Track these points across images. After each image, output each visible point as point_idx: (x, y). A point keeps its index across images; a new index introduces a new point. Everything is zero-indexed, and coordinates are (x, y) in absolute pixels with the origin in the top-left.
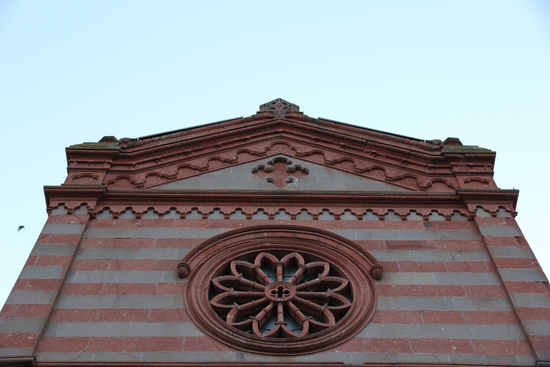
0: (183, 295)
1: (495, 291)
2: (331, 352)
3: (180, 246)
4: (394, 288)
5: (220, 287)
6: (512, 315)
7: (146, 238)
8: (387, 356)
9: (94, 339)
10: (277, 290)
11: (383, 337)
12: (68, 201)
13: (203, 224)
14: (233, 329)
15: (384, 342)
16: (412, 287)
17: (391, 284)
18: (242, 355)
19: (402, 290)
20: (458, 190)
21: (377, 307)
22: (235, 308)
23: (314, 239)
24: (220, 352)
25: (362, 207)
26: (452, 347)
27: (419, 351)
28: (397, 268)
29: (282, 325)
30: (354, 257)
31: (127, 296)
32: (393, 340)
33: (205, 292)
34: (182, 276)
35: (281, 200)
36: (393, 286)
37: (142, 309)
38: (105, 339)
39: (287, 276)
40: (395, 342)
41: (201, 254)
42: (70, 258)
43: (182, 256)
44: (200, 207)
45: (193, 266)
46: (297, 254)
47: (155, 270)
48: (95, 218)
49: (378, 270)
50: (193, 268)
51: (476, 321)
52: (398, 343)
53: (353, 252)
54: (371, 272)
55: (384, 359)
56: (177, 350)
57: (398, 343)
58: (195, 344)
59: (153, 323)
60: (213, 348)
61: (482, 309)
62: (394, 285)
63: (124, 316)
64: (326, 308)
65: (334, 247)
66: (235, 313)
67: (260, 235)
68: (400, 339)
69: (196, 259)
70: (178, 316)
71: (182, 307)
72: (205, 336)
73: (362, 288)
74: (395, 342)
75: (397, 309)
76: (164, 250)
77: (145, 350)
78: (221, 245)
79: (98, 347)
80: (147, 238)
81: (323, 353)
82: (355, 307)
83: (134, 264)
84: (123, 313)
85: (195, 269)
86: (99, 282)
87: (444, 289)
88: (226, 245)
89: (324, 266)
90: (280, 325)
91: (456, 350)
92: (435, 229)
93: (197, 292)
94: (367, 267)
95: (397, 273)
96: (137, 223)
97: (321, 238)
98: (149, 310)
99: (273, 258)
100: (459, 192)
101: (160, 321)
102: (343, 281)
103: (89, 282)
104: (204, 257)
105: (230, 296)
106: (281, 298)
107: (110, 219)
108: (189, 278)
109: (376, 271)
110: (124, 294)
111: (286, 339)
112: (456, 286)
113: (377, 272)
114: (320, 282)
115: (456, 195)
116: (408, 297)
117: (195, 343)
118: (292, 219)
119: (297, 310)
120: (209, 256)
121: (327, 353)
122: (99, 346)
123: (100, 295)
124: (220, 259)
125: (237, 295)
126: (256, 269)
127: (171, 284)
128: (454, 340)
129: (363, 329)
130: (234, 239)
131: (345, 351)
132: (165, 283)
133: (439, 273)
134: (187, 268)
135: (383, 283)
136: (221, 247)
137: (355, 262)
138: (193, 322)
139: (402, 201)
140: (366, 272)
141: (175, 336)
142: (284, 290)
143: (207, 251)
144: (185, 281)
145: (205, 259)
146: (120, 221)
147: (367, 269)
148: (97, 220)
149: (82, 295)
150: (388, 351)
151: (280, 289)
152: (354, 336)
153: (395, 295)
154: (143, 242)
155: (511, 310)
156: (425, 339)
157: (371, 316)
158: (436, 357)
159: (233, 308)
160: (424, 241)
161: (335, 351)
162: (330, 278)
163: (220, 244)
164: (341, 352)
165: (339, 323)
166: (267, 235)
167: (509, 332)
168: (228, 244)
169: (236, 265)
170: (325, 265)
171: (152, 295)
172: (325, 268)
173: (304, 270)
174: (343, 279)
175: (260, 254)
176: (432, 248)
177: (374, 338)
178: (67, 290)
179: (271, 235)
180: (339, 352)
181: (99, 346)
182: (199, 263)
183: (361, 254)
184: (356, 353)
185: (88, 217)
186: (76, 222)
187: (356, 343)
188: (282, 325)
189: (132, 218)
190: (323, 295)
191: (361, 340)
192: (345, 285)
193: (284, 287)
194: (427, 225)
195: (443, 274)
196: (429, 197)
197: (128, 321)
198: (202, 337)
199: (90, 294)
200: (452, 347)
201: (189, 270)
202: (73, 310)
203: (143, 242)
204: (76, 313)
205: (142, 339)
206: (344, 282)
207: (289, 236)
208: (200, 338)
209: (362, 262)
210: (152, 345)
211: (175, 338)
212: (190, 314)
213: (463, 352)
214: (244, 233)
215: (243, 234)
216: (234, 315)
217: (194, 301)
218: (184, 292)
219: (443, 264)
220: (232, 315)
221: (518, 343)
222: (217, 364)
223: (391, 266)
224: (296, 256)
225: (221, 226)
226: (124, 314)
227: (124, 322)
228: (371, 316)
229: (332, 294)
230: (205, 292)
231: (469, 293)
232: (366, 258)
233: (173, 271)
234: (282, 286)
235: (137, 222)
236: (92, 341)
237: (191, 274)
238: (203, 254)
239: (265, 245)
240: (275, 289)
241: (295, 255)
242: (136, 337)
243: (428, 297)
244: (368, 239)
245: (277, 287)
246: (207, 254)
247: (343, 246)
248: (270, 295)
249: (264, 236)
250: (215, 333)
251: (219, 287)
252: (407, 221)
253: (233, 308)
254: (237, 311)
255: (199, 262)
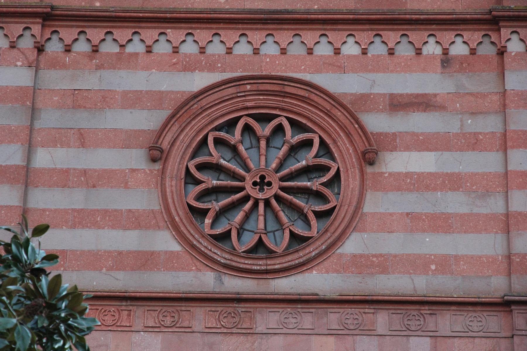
0: (157, 190)
1: (497, 182)
2: (308, 273)
3: (149, 104)
4: (386, 178)
5: (196, 176)
6: (505, 219)
7: (108, 90)
8: (364, 278)
9: (73, 252)
10: (258, 181)
11: (363, 252)
12: (7, 24)
13: (174, 64)
14: (212, 240)
15: (363, 260)
16: (406, 176)
17: (384, 170)
18: (221, 277)
19: (395, 182)
20: (491, 10)
21: (364, 209)
22: (213, 209)
23: (305, 96)
24: (199, 273)
25: (369, 31)
26: (431, 265)
27: (397, 272)
28: (395, 144)
29: (261, 234)
30: (348, 127)
31: (97, 190)
32: (374, 256)
33: (181, 182)
34: (154, 160)
35: (269, 21)
36: (386, 175)
37: (116, 210)
38: (83, 252)
39: (271, 147)
40: (375, 259)
41: (174, 125)
42: (28, 131)
43: (152, 123)
44: (169, 32)
45: (165, 145)
46: (284, 120)
47: (124, 148)
48: (43, 50)
49: (371, 155)
50: (165, 148)
51: (464, 228)
52: (377, 261)
53: (348, 121)
54: (364, 154)
55: (361, 283)
56: (156, 270)
57: (377, 261)
58: (173, 261)
59: (129, 231)
60: (191, 267)
61: (476, 210)
62: (387, 172)
63: (98, 221)
64: (310, 209)
65: (327, 110)
66: (213, 216)
67: (242, 88)
68: (381, 255)
69: (169, 133)
70: (154, 221)
71: (157, 208)
72: (183, 250)
73: (351, 179)
74: (375, 259)
75: (384, 211)
76: (131, 112)
77: (124, 269)
78: (196, 108)
79: (78, 265)
80: (110, 90)
81: (300, 274)
82: (341, 206)
83: (100, 137)
84: (97, 215)
85: (169, 147)
86: (65, 167)
87: (441, 179)
88: (202, 106)
89: (313, 139)
90: (259, 234)
91: (435, 269)
92: (452, 72)
93: (172, 186)
94: (361, 148)
95: (394, 153)
96: (94, 61)
97: (313, 95)
98: (123, 211)
99: (256, 127)
100: (493, 13)
101: (136, 228)
102: (332, 166)
103: (54, 167)
104: (177, 128)
105: (208, 188)
106: (263, 193)
107: (61, 52)
108: (163, 161)
109: (369, 157)
110: (94, 186)
111: (264, 256)
112: (456, 174)
113: (369, 158)
114: (306, 166)
115: (489, 13)
116: (400, 192)
117: (173, 260)
118: (281, 54)
119: (279, 211)
120: (183, 125)
121: (304, 274)
122: (79, 263)
123: (69, 187)
124: (195, 131)
125: (215, 187)
126: (236, 145)
127: (143, 171)
128: (435, 255)
129: (344, 242)
130: (211, 96)
131: (323, 272)
132: (137, 170)
133: (440, 153)
134: (160, 151)
135: (375, 169)
136: (196, 110)
137: (348, 135)
138: (170, 231)
139: (420, 22)
140: (359, 152)
141: (152, 250)
142: (266, 181)
143: (180, 119)
144: (158, 166)
145: (179, 130)
146: (75, 56)
147: (361, 148)
148: (46, 54)
149: (50, 187)
150: (365, 272)
151: (262, 178)
152: (334, 252)
153: (386, 189)
154: (106, 97)
155: (505, 212)
156: (407, 255)
157: (356, 222)
158: (413, 280)
159: (211, 208)
160: (435, 95)
161: (313, 271)
162: (318, 160)
163: (196, 106)
164: (318, 273)
165: (320, 233)
166: (251, 87)
167: (494, 244)
168: (204, 105)
169: (214, 137)
170: (314, 137)
171: (125, 188)
172: (314, 143)
173: (290, 147)
174: (333, 163)
175: (242, 119)
176: (442, 108)
177: (354, 254)
178: (32, 179)
179: (255, 87)
180: (316, 273)
181: (79, 263)
182: (172, 137)
183: (356, 126)
184: (334, 275)
185: (36, 51)
186: (23, 64)
187: (335, 261)
188: (261, 234)
189: (88, 51)
190: (308, 187)
191: (341, 255)
192: (334, 173)
193: (266, 176)
194: (445, 64)
195: (447, 155)
196: (454, 16)
197: (103, 228)
198: (180, 251)
199: (58, 186)
200: (431, 265)
201: (162, 151)
202: (44, 210)
203: (106, 97)
204: (48, 215)
205: (120, 253)
206: (333, 166)
207: (275, 90)
208: (178, 252)
209: (356, 137)
210: (131, 262)
211: (153, 253)
212: (166, 220)
213: (441, 272)
214: (223, 87)
215: (221, 88)
216: (212, 218)
217: (170, 200)
218: (158, 185)
219: (449, 135)
220: (209, 219)
221: (499, 260)
222: (196, 295)
223: (389, 140)
224: (282, 122)
225: (196, 67)
226: (98, 217)
227: (99, 229)
228: (356, 222)
229: (318, 187)
230: (181, 182)
231: (468, 186)
232: (361, 134)
233: (144, 149)
234: (264, 173)
235: (95, 58)
236: (71, 256)
237: (164, 156)
238: (176, 123)
239: (247, 106)
240: (257, 178)
241: (282, 120)
242: (114, 251)
243: (421, 192)
244: (369, 92)
245: (259, 175)
246: (181, 124)
247: (337, 111)
248: (251, 187)
249: (246, 90)
250: (193, 247)
251: (195, 175)
252: (422, 55)
253: (211, 208)
254: (215, 212)
255: (172, 136)
